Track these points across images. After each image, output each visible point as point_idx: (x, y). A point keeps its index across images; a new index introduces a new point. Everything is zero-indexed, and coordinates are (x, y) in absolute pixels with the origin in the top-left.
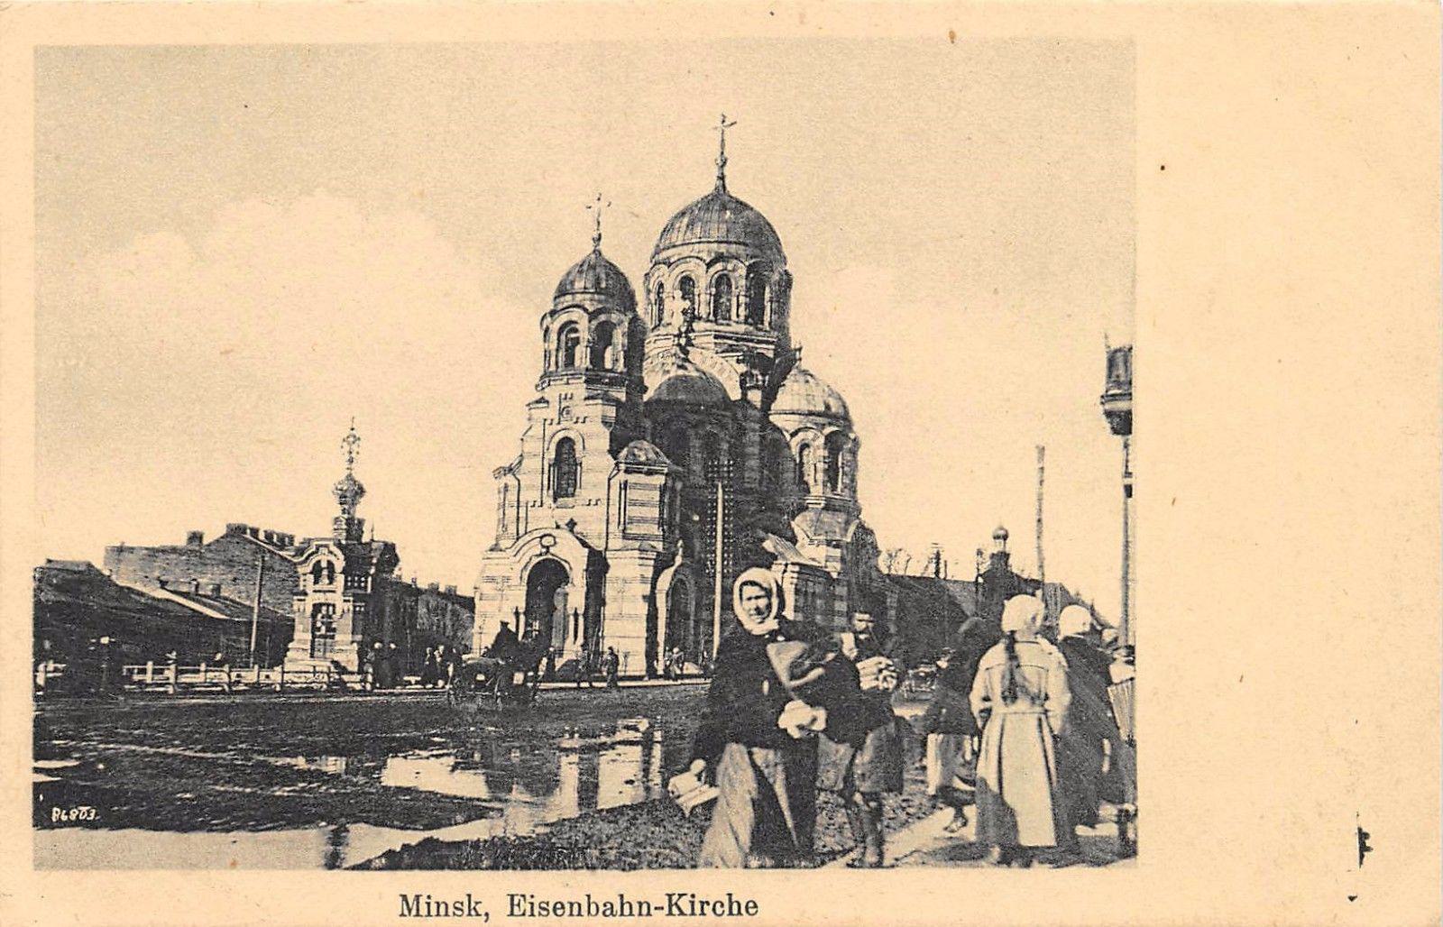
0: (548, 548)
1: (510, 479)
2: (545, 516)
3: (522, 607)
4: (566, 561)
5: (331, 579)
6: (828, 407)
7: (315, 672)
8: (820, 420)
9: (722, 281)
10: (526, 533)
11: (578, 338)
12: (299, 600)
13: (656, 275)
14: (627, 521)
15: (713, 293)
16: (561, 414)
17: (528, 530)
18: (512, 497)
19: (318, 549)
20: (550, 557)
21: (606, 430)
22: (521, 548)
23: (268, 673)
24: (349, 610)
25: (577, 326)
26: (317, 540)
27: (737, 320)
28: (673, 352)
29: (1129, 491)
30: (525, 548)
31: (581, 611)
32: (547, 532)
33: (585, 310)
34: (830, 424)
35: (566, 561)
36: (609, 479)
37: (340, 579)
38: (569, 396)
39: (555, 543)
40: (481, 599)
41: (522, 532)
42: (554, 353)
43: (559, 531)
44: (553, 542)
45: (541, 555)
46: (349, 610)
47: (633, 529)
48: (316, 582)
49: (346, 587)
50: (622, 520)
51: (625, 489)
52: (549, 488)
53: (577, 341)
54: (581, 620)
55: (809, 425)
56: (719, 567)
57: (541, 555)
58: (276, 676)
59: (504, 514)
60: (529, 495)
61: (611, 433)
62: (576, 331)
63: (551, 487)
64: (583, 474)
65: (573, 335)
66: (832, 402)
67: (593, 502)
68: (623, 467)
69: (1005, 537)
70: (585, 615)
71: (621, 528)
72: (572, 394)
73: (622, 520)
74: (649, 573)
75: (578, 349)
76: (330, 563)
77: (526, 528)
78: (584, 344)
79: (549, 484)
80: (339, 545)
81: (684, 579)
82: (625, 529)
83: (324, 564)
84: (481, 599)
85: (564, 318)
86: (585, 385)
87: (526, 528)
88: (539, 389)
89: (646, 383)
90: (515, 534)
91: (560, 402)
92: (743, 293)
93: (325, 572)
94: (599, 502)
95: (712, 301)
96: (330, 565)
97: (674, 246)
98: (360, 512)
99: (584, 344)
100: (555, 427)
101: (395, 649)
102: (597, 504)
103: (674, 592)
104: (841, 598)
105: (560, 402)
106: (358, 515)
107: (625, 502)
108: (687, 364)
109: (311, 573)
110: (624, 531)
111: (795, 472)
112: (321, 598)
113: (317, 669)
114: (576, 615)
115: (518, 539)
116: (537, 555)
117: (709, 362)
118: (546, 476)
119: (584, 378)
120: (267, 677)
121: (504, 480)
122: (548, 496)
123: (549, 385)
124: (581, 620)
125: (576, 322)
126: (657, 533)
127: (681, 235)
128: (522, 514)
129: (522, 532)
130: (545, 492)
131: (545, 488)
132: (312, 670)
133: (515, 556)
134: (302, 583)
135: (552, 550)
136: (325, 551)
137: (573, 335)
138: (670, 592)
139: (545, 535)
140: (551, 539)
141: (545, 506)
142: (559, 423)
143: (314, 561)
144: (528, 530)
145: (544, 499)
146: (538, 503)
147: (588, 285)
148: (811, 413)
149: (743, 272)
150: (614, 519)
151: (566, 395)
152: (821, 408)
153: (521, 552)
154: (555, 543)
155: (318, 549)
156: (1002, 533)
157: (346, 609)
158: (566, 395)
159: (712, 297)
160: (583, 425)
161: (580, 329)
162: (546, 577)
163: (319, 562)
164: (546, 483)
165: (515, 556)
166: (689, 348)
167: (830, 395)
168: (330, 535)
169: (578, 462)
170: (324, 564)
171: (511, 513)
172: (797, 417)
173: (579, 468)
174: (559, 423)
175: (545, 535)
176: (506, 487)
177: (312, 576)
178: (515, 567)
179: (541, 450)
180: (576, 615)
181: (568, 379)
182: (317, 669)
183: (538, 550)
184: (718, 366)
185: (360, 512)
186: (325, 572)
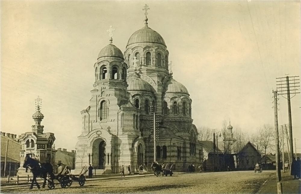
0: (99, 135)
1: (86, 114)
2: (97, 125)
3: (91, 153)
4: (105, 139)
5: (33, 146)
6: (181, 91)
7: (28, 177)
8: (179, 94)
9: (148, 53)
10: (92, 131)
11: (106, 70)
12: (22, 153)
13: (128, 52)
14: (124, 126)
15: (146, 57)
16: (102, 93)
17: (92, 130)
18: (87, 119)
19: (28, 136)
20: (100, 138)
21: (116, 98)
22: (91, 135)
23: (11, 178)
24: (39, 156)
25: (105, 67)
26: (27, 133)
27: (153, 65)
28: (134, 75)
29: (230, 122)
30: (92, 135)
31: (110, 154)
32: (98, 130)
33: (109, 62)
34: (183, 96)
35: (105, 139)
36: (118, 113)
37: (36, 146)
38: (104, 88)
39: (101, 133)
40: (78, 152)
41: (90, 130)
42: (99, 75)
43: (102, 130)
44: (100, 133)
45: (97, 137)
46: (39, 156)
47: (125, 129)
48: (27, 147)
49: (38, 148)
50: (122, 126)
51: (123, 116)
52: (98, 116)
53: (106, 71)
54: (110, 157)
55: (176, 96)
56: (155, 139)
57: (97, 137)
58: (15, 178)
59: (85, 125)
60: (93, 119)
61: (118, 99)
62: (106, 68)
63: (99, 116)
64: (109, 112)
65: (104, 69)
66: (182, 89)
67: (113, 120)
68: (122, 109)
69: (232, 128)
70: (111, 155)
71: (122, 128)
72: (105, 87)
73: (122, 126)
74: (131, 142)
75: (106, 74)
76: (32, 140)
77: (92, 129)
78: (108, 72)
79: (98, 115)
80: (34, 134)
81: (142, 143)
82: (123, 128)
83: (30, 141)
84: (78, 152)
85: (102, 64)
86: (109, 85)
87: (92, 129)
88: (95, 86)
89: (128, 84)
90: (88, 131)
91: (102, 90)
92: (155, 57)
93: (30, 144)
94: (115, 120)
95: (145, 59)
96: (32, 140)
97: (134, 43)
98: (42, 124)
99: (108, 72)
100: (100, 98)
101: (41, 168)
102: (114, 121)
103: (139, 147)
104: (188, 148)
105: (102, 90)
106: (42, 124)
107: (123, 120)
108: (139, 79)
109: (26, 144)
110: (123, 129)
111: (172, 110)
112: (29, 152)
113: (29, 176)
114: (108, 155)
115: (89, 133)
116: (96, 138)
117: (145, 78)
118: (98, 113)
119: (109, 83)
120: (12, 179)
121: (84, 114)
122: (98, 119)
123: (98, 85)
124: (110, 157)
125: (105, 65)
126: (133, 129)
127: (135, 40)
128: (90, 125)
129: (90, 130)
130: (97, 118)
131: (98, 116)
132: (27, 176)
133: (89, 138)
134: (22, 147)
135: (100, 136)
136: (31, 136)
137: (104, 69)
138: (138, 147)
139: (98, 131)
140: (100, 132)
141: (98, 122)
142: (101, 96)
143: (27, 139)
144: (92, 130)
145: (97, 120)
146: (95, 121)
147: (109, 54)
148: (176, 93)
149: (154, 51)
150: (120, 125)
151: (103, 88)
152: (180, 91)
153: (91, 136)
154: (101, 133)
155: (28, 136)
156: (231, 127)
157: (38, 155)
158: (103, 88)
159: (145, 59)
160: (109, 97)
161: (107, 68)
162: (100, 145)
163: (29, 140)
164: (97, 114)
165: (89, 138)
166: (140, 74)
167: (182, 87)
168: (32, 131)
169: (108, 108)
170: (30, 141)
171: (87, 124)
172: (172, 94)
173: (108, 110)
174: (101, 96)
175: (98, 131)
176: (85, 116)
177: (26, 145)
178: (88, 142)
179: (96, 105)
180: (108, 155)
181: (104, 83)
182: (29, 176)
183: (96, 136)
184: (148, 79)
185: (42, 124)
186: (30, 144)
